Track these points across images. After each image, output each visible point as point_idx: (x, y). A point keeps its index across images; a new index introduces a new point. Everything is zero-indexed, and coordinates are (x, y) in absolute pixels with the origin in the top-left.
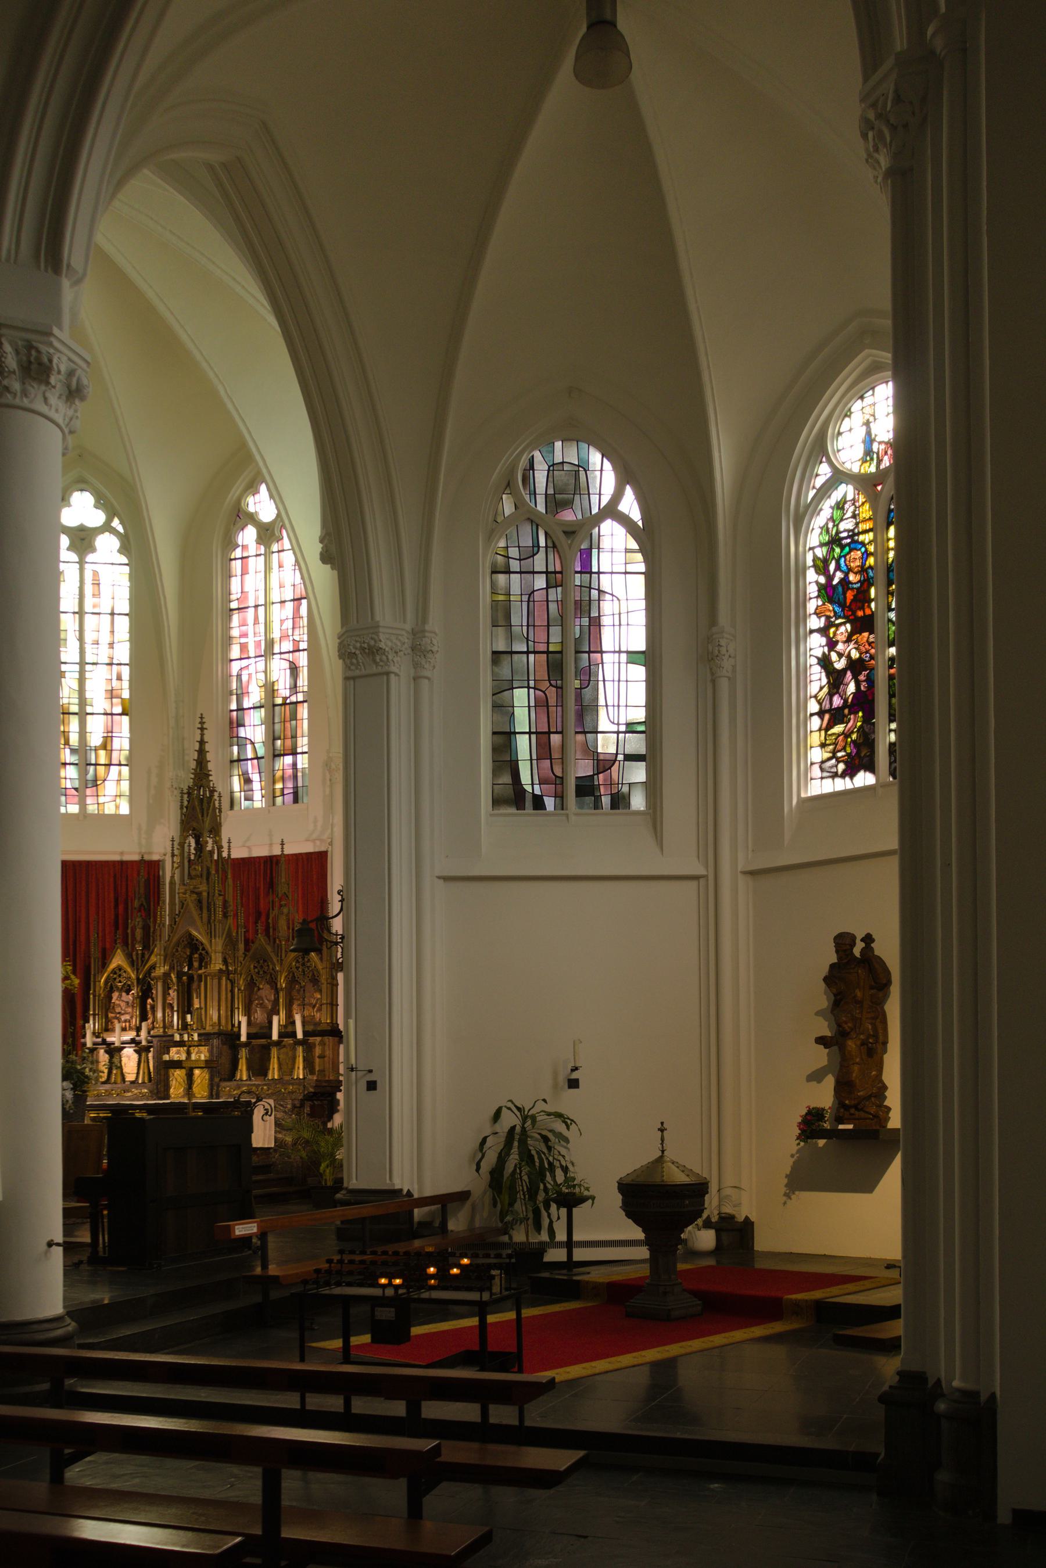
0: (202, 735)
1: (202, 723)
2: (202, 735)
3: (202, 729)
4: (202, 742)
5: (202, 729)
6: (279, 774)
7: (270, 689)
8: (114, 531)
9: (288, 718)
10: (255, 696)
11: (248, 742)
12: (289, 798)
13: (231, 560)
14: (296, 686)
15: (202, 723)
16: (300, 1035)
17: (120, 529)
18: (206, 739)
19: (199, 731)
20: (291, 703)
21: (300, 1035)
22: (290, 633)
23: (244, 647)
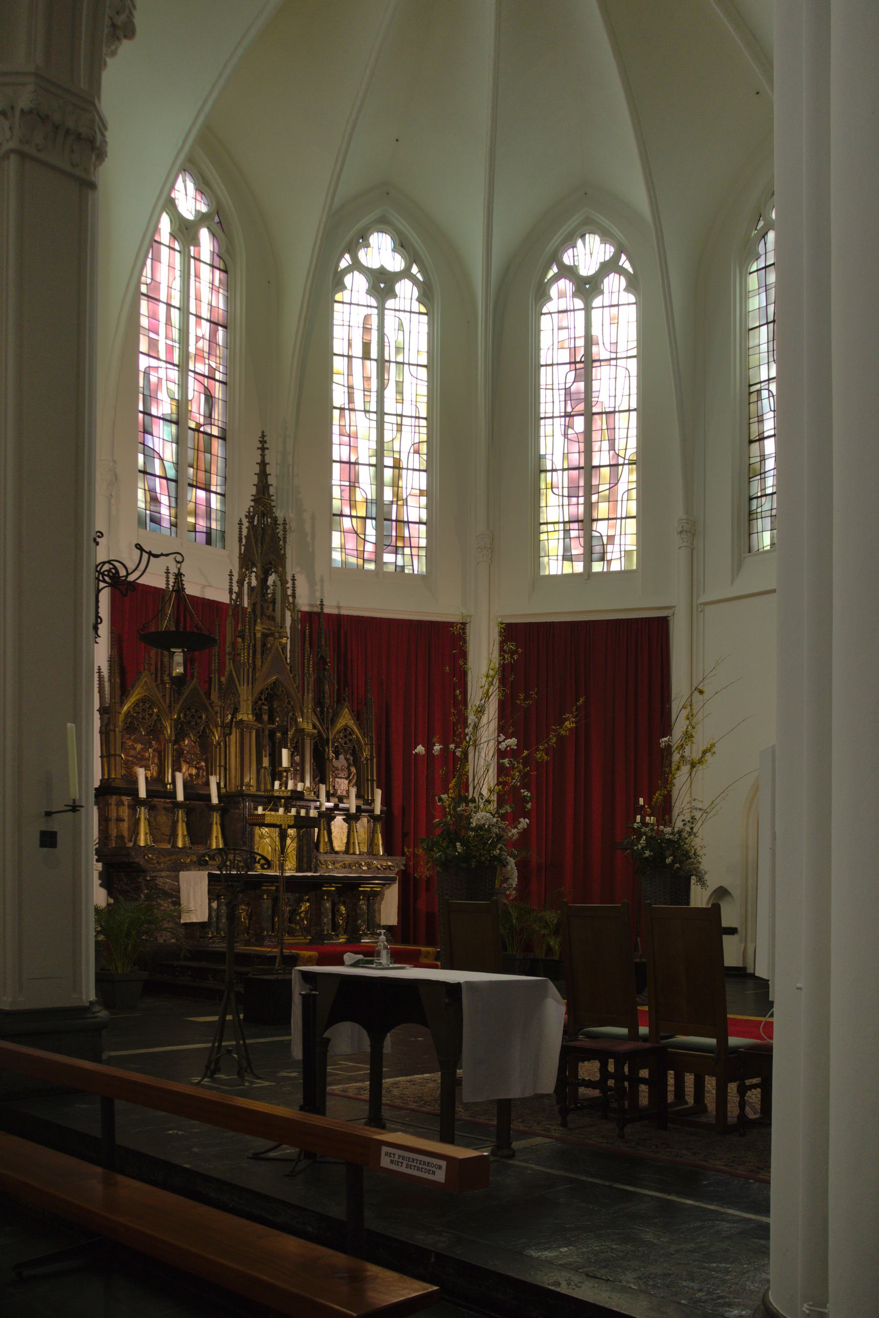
0: (263, 455)
1: (263, 442)
2: (263, 455)
3: (263, 449)
4: (263, 464)
5: (263, 449)
6: (191, 506)
7: (182, 404)
8: (621, 271)
9: (202, 448)
10: (164, 407)
11: (156, 455)
12: (202, 538)
13: (542, 314)
14: (210, 417)
15: (263, 442)
16: (143, 794)
17: (627, 266)
18: (267, 461)
19: (260, 452)
20: (204, 433)
21: (143, 794)
22: (170, 342)
23: (153, 344)
